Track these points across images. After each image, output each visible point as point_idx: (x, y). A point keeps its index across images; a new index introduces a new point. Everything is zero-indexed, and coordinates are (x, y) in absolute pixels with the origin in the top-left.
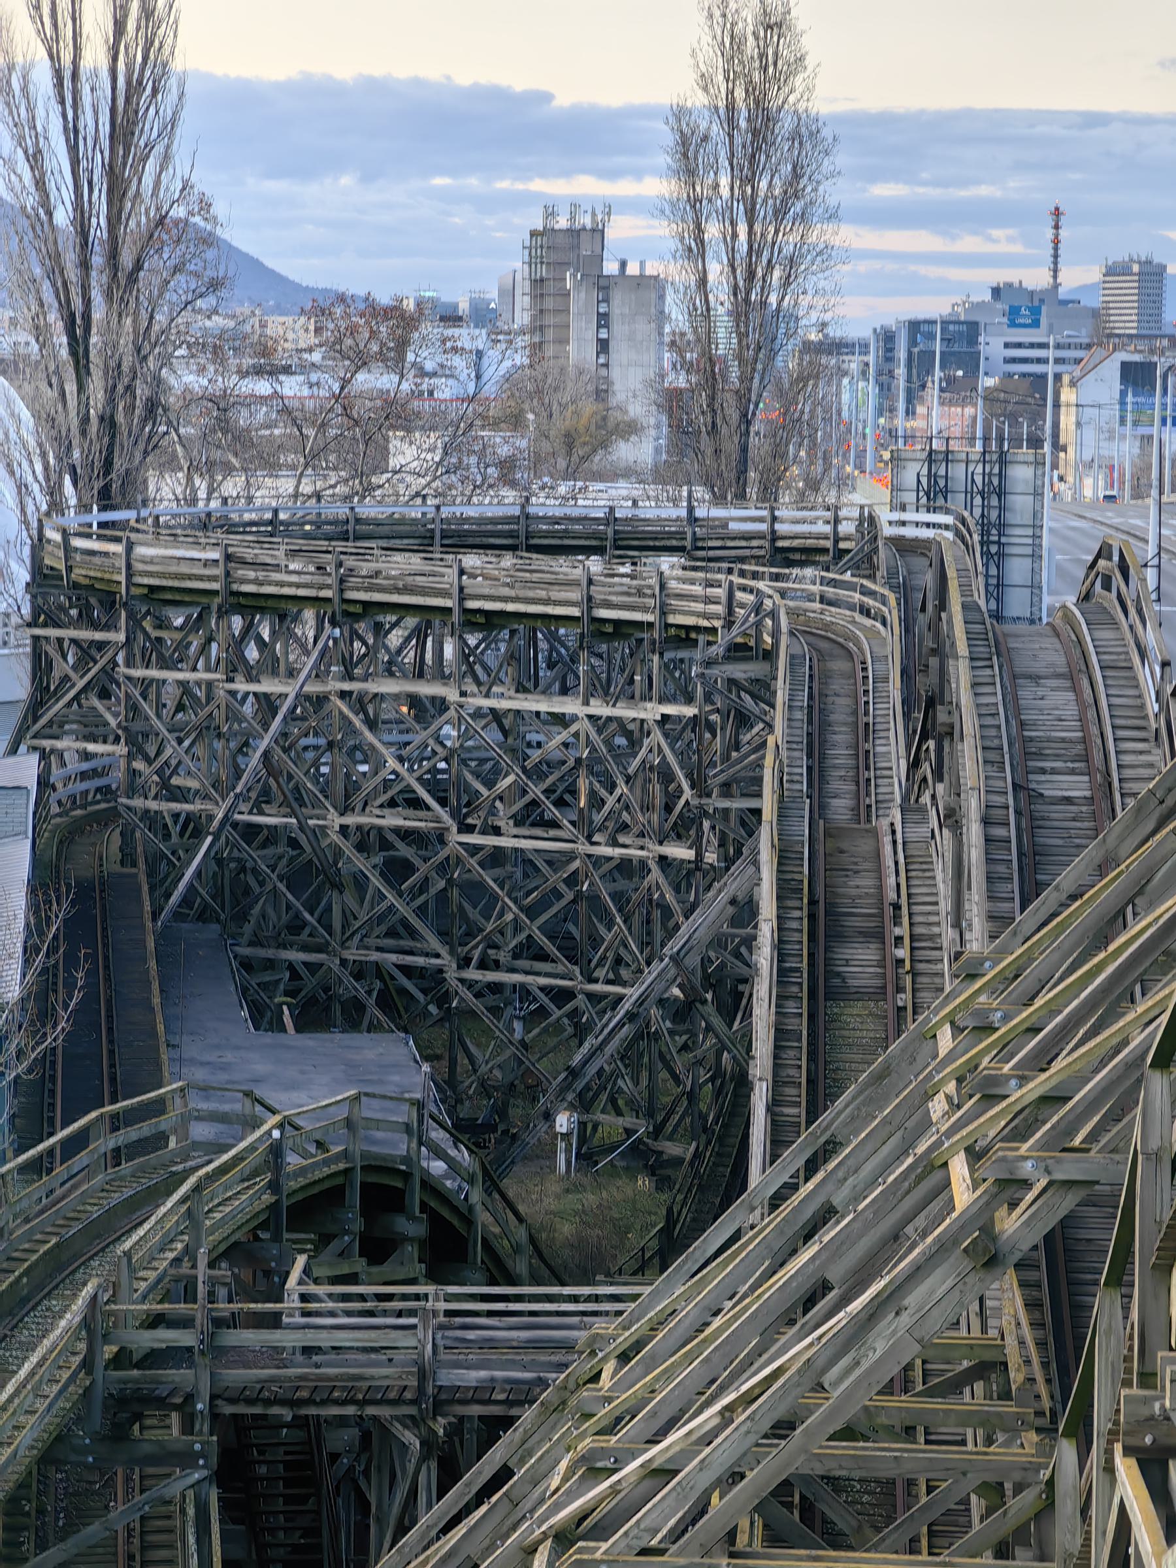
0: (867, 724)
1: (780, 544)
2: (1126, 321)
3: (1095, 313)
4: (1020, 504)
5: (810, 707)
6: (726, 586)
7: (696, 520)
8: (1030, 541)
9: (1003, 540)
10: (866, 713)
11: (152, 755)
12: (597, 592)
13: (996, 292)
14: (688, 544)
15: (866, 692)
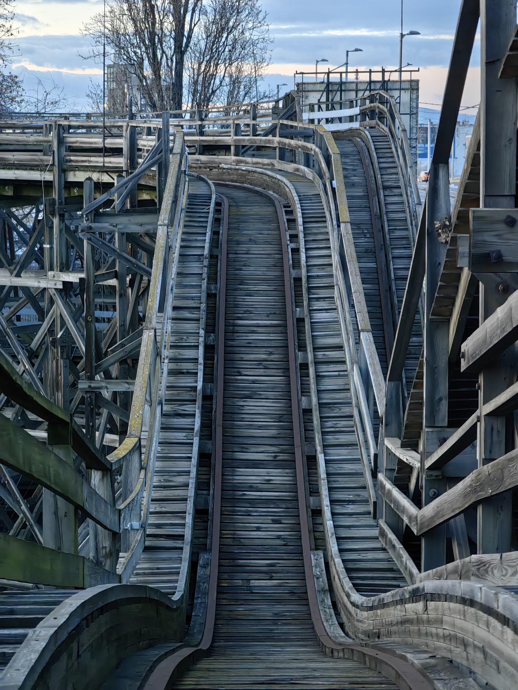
0: (298, 280)
5: (213, 257)
6: (126, 133)
10: (296, 264)
15: (294, 237)
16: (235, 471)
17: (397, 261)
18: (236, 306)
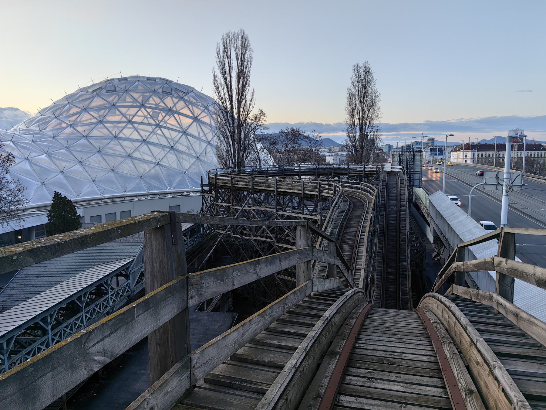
1: (366, 173)
2: (430, 144)
3: (427, 143)
4: (417, 164)
6: (334, 186)
8: (419, 171)
13: (415, 142)
14: (348, 173)
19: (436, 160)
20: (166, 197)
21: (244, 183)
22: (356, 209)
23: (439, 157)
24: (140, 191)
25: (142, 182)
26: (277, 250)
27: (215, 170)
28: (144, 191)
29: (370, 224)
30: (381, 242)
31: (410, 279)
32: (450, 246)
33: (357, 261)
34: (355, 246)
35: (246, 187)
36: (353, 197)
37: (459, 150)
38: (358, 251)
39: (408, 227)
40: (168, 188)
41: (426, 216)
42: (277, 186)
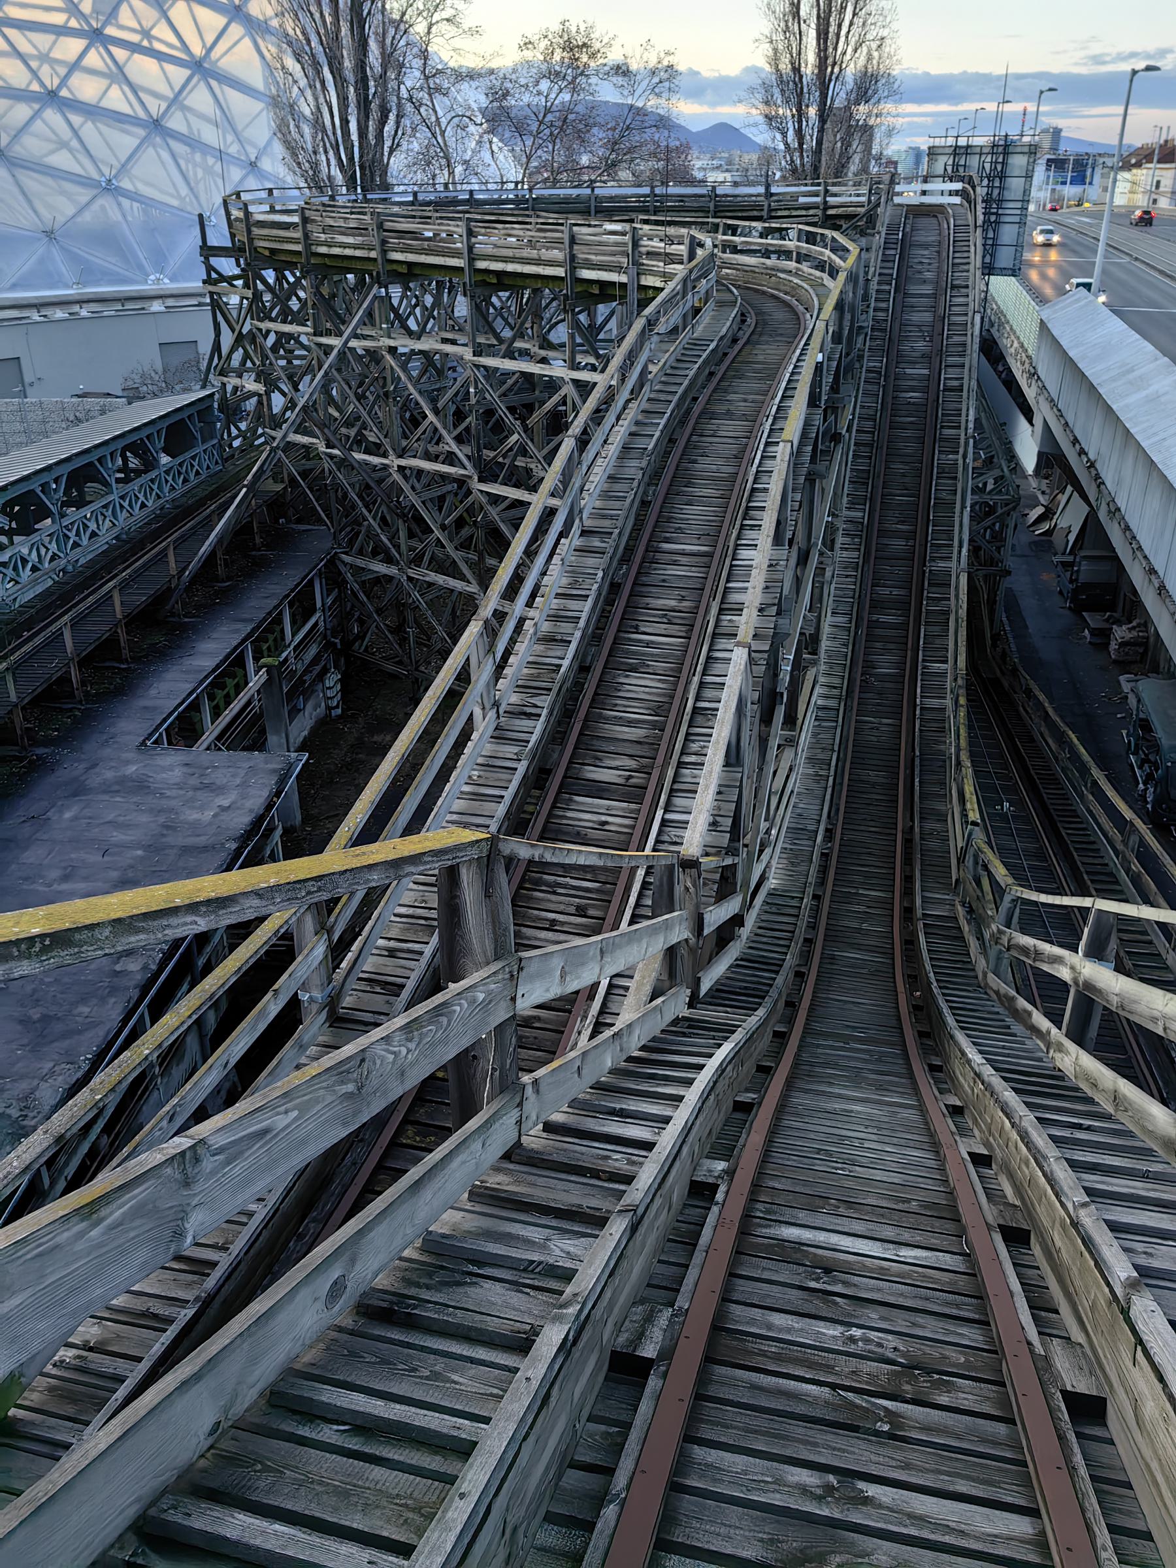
1: (830, 212)
4: (1015, 184)
6: (687, 241)
7: (772, 195)
8: (1019, 212)
9: (1000, 211)
11: (256, 398)
12: (581, 253)
14: (765, 214)
16: (571, 800)
17: (949, 370)
18: (669, 520)
19: (1061, 199)
20: (143, 309)
21: (350, 240)
22: (764, 338)
23: (1070, 191)
24: (52, 286)
25: (55, 252)
26: (482, 508)
27: (264, 194)
28: (67, 286)
29: (813, 401)
30: (860, 479)
31: (963, 633)
32: (1102, 487)
33: (727, 590)
34: (730, 509)
35: (358, 253)
36: (764, 293)
37: (1138, 165)
38: (739, 537)
39: (971, 415)
40: (153, 277)
41: (1022, 381)
42: (470, 248)
